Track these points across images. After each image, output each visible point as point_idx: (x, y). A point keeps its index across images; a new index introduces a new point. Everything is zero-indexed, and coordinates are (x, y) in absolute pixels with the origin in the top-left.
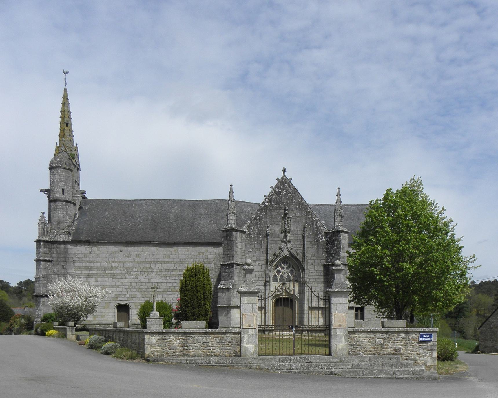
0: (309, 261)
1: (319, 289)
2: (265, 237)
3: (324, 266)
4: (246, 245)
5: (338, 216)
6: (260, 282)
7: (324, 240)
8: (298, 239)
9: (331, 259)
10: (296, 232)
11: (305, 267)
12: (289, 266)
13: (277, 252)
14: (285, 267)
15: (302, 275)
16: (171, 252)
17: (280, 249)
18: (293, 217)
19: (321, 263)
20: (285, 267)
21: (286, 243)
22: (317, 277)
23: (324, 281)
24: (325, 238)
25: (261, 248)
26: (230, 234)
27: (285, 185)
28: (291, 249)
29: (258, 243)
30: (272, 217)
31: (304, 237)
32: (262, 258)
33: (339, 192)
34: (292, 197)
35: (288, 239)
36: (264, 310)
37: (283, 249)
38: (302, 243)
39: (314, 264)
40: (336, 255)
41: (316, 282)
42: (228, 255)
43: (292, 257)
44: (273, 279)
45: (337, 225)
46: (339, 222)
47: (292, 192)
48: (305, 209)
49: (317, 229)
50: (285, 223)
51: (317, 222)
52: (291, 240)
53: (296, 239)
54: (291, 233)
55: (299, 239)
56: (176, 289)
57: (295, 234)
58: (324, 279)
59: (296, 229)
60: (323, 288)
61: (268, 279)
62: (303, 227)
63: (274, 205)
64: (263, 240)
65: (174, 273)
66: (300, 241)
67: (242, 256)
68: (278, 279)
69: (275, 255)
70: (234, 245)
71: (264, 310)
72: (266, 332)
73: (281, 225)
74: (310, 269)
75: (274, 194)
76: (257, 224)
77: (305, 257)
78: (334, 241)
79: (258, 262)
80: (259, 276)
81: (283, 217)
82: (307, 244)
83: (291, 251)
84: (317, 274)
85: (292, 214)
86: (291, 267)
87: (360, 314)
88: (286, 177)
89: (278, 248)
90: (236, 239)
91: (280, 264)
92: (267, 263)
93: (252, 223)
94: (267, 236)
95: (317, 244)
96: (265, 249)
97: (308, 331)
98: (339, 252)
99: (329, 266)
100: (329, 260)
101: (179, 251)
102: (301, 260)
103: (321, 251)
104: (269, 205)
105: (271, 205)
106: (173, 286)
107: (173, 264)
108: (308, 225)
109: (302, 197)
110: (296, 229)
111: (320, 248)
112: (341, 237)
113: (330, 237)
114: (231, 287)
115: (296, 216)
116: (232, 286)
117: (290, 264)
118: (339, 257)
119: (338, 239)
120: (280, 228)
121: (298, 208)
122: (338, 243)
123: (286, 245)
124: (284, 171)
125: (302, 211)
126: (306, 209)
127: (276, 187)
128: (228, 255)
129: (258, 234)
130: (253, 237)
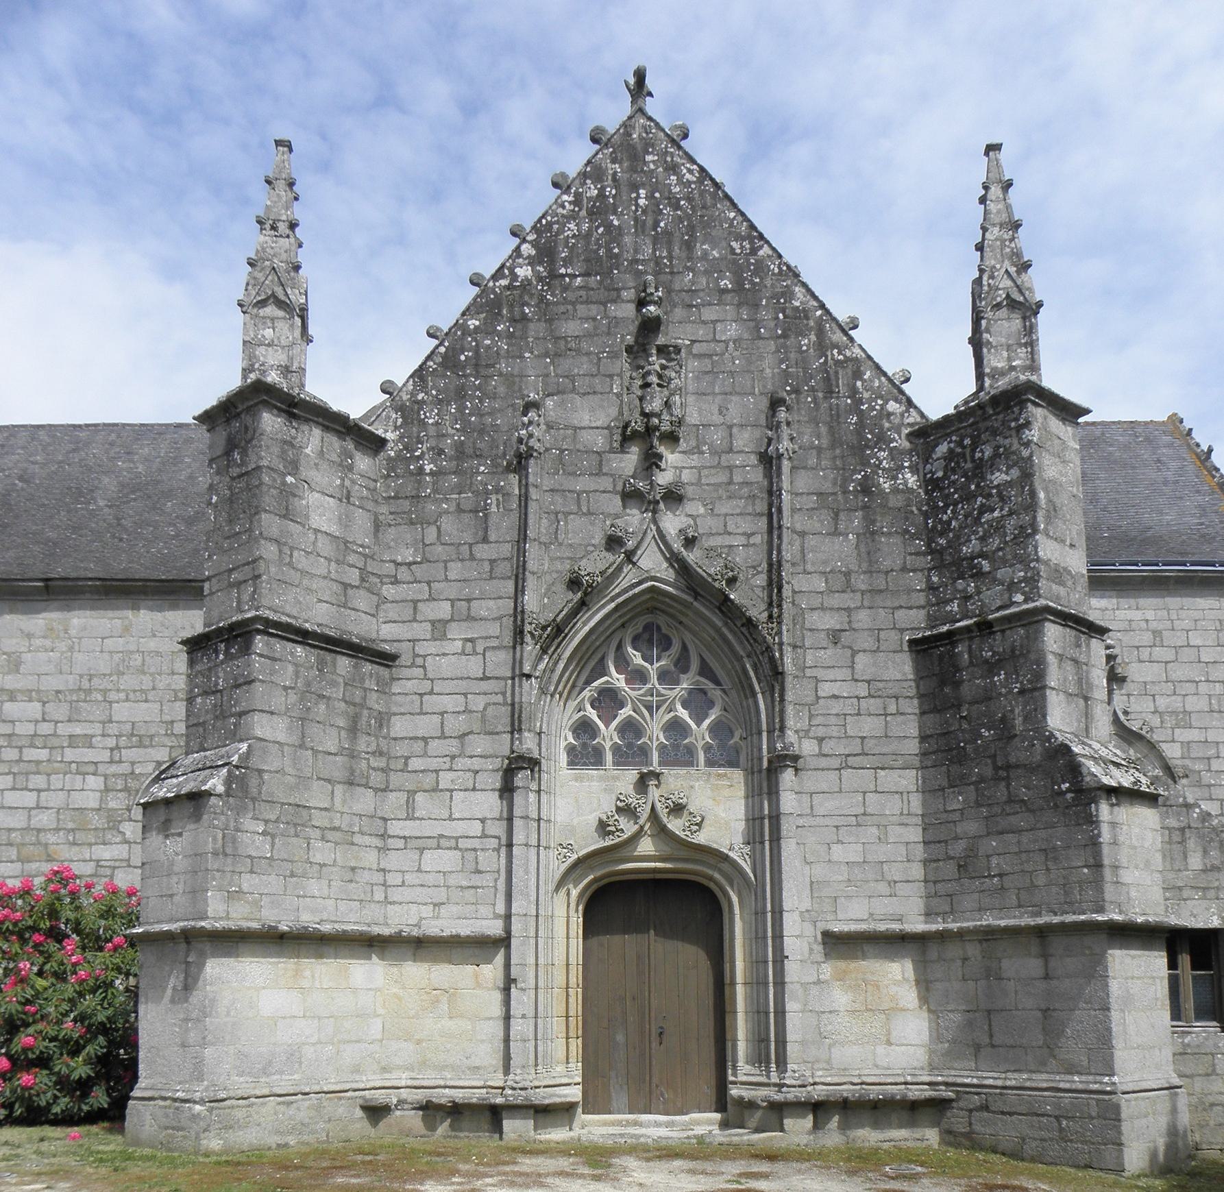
0: (814, 619)
1: (893, 806)
2: (508, 469)
3: (920, 647)
4: (377, 526)
5: (1003, 313)
6: (476, 763)
7: (912, 480)
8: (731, 482)
9: (967, 598)
10: (717, 437)
11: (788, 660)
12: (682, 664)
13: (595, 564)
14: (652, 670)
15: (770, 717)
16: (29, 636)
17: (613, 542)
18: (697, 349)
19: (894, 636)
20: (652, 670)
21: (652, 506)
22: (870, 726)
23: (924, 754)
24: (914, 469)
25: (485, 540)
26: (246, 428)
27: (645, 163)
28: (690, 542)
29: (460, 510)
30: (560, 349)
31: (769, 462)
32: (482, 608)
33: (994, 167)
34: (691, 229)
35: (663, 478)
36: (500, 959)
37: (630, 544)
38: (761, 506)
39: (845, 638)
40: (1005, 562)
41: (865, 761)
42: (230, 571)
43: (696, 595)
44: (571, 750)
45: (994, 369)
46: (1009, 347)
47: (689, 199)
48: (776, 296)
49: (860, 414)
50: (646, 385)
51: (858, 375)
52: (690, 491)
53: (722, 478)
54: (683, 445)
55: (738, 478)
56: (46, 845)
57: (714, 452)
58: (923, 738)
59: (717, 419)
60: (916, 803)
61: (528, 743)
62: (764, 403)
63: (573, 276)
64: (497, 490)
65: (43, 754)
66: (745, 491)
67: (346, 586)
68: (608, 745)
69: (574, 583)
70: (269, 499)
71: (500, 959)
72: (507, 1124)
73: (618, 395)
74: (820, 673)
75: (573, 216)
76: (460, 394)
77: (787, 592)
78: (980, 469)
79: (457, 632)
80: (464, 728)
81: (629, 349)
82: (794, 511)
83: (692, 557)
84: (874, 705)
85: (689, 327)
86: (695, 665)
87: (1194, 977)
88: (650, 119)
89: (598, 538)
90: (294, 466)
91: (620, 647)
92: (519, 634)
93: (424, 389)
94: (520, 462)
95: (865, 507)
96: (507, 549)
97: (819, 1109)
98: (1026, 533)
99: (953, 644)
100: (955, 607)
101: (73, 632)
102: (757, 612)
103: (892, 551)
104: (540, 279)
105: (553, 275)
106: (28, 829)
107: (38, 705)
108: (796, 391)
109: (752, 227)
110: (717, 419)
111: (889, 534)
112: (1034, 434)
113: (951, 456)
114: (216, 783)
115: (715, 340)
116: (228, 782)
117: (685, 648)
118: (1027, 568)
119: (1008, 452)
120: (614, 412)
121: (724, 291)
122: (1015, 473)
123: (655, 521)
124: (639, 88)
125: (756, 306)
126: (783, 294)
127: (583, 175)
128: (230, 571)
129: (461, 452)
130: (432, 473)
